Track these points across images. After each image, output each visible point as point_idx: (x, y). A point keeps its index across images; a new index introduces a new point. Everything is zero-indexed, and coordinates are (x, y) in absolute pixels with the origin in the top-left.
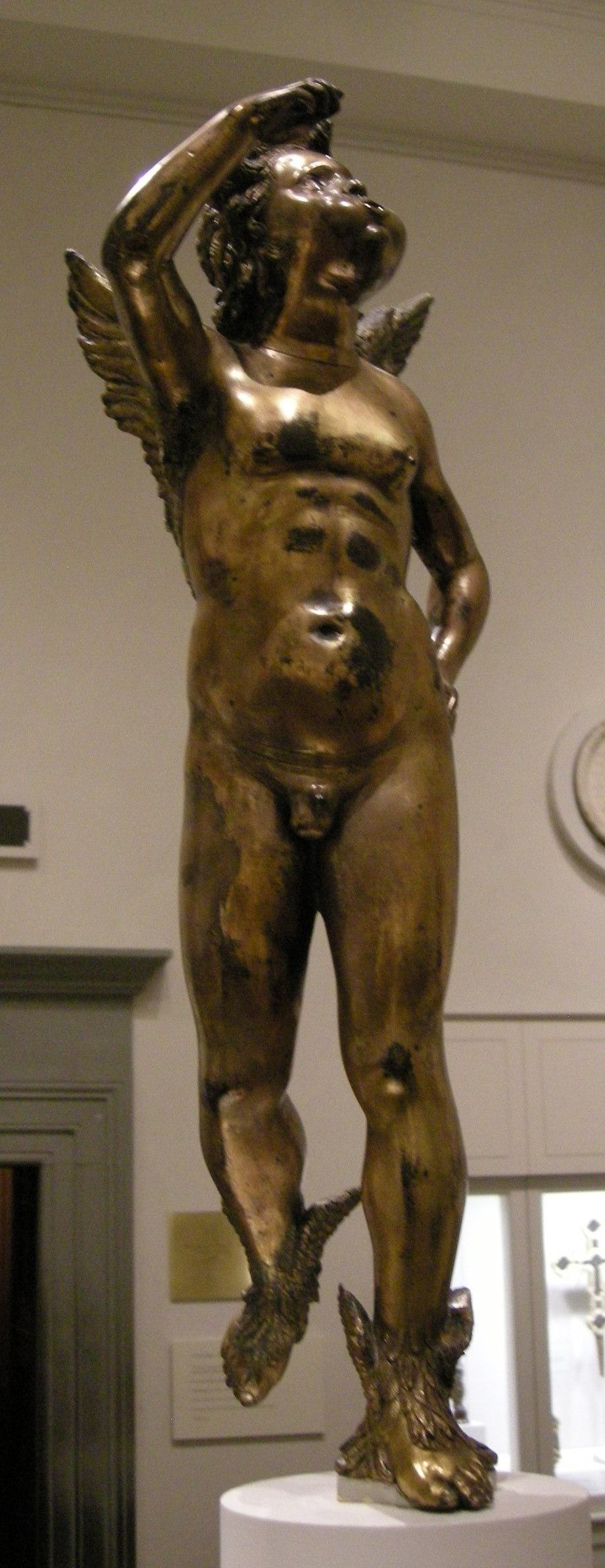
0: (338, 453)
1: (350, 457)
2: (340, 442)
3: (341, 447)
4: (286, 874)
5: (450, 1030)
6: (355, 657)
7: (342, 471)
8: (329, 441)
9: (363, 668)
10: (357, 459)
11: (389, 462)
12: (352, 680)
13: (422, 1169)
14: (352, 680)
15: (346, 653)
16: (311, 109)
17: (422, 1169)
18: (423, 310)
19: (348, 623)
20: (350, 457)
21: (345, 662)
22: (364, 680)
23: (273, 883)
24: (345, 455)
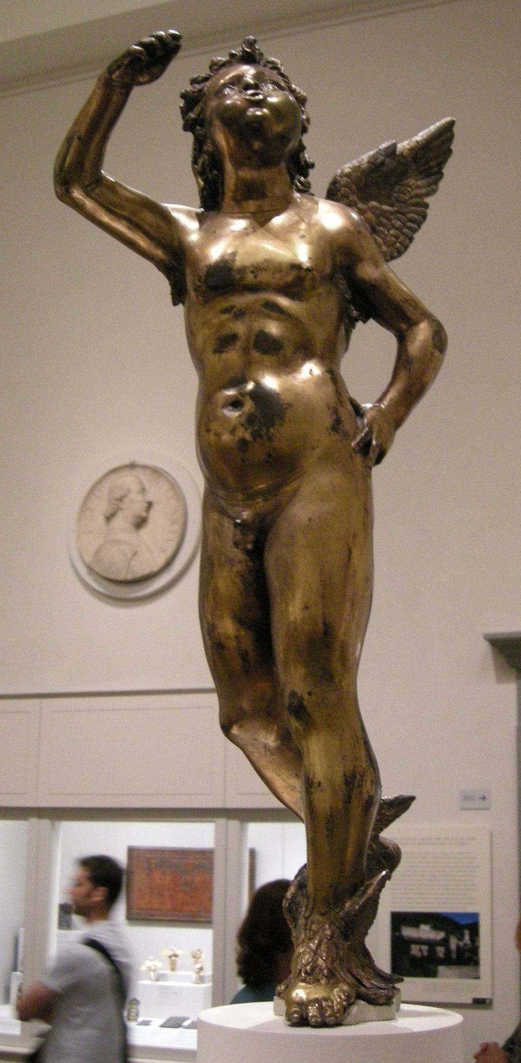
0: (250, 277)
1: (259, 278)
2: (251, 269)
3: (252, 272)
4: (242, 576)
5: (210, 683)
6: (250, 420)
7: (254, 288)
8: (242, 270)
9: (256, 428)
10: (264, 277)
11: (287, 274)
12: (248, 436)
13: (316, 781)
14: (248, 436)
15: (243, 420)
16: (160, 53)
17: (316, 781)
18: (445, 135)
19: (248, 398)
20: (259, 278)
21: (242, 425)
22: (256, 435)
23: (234, 583)
24: (255, 277)
